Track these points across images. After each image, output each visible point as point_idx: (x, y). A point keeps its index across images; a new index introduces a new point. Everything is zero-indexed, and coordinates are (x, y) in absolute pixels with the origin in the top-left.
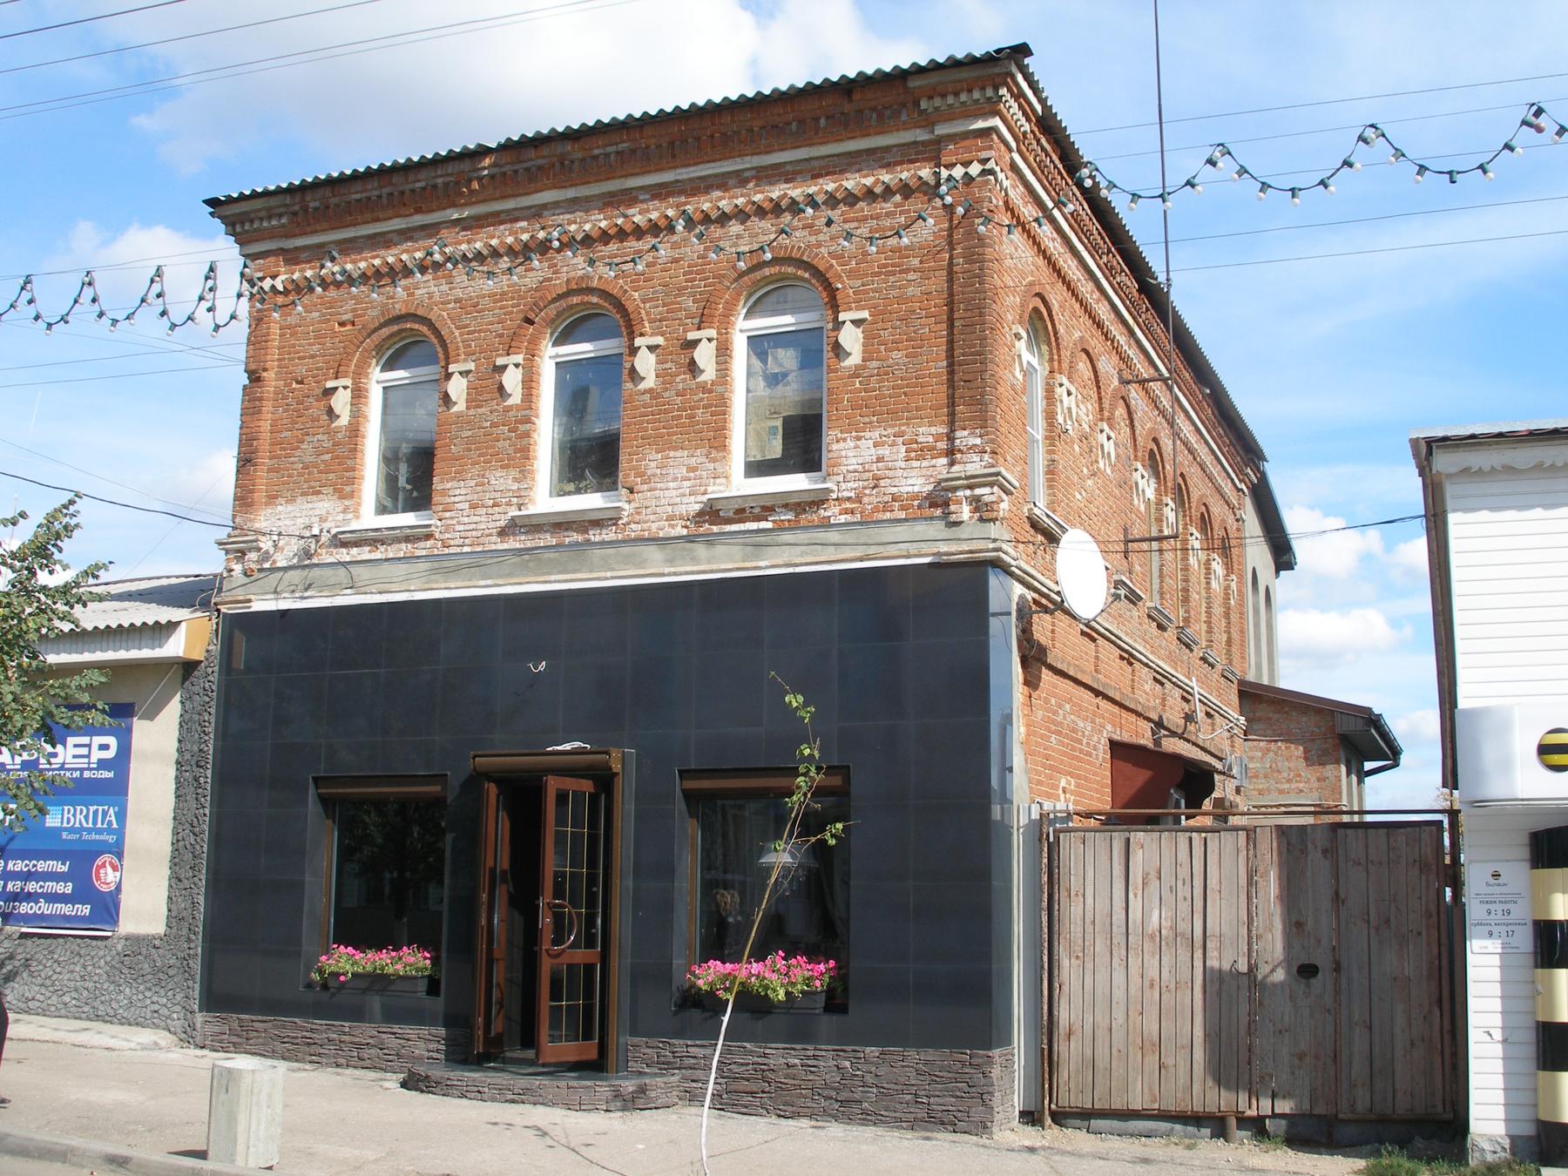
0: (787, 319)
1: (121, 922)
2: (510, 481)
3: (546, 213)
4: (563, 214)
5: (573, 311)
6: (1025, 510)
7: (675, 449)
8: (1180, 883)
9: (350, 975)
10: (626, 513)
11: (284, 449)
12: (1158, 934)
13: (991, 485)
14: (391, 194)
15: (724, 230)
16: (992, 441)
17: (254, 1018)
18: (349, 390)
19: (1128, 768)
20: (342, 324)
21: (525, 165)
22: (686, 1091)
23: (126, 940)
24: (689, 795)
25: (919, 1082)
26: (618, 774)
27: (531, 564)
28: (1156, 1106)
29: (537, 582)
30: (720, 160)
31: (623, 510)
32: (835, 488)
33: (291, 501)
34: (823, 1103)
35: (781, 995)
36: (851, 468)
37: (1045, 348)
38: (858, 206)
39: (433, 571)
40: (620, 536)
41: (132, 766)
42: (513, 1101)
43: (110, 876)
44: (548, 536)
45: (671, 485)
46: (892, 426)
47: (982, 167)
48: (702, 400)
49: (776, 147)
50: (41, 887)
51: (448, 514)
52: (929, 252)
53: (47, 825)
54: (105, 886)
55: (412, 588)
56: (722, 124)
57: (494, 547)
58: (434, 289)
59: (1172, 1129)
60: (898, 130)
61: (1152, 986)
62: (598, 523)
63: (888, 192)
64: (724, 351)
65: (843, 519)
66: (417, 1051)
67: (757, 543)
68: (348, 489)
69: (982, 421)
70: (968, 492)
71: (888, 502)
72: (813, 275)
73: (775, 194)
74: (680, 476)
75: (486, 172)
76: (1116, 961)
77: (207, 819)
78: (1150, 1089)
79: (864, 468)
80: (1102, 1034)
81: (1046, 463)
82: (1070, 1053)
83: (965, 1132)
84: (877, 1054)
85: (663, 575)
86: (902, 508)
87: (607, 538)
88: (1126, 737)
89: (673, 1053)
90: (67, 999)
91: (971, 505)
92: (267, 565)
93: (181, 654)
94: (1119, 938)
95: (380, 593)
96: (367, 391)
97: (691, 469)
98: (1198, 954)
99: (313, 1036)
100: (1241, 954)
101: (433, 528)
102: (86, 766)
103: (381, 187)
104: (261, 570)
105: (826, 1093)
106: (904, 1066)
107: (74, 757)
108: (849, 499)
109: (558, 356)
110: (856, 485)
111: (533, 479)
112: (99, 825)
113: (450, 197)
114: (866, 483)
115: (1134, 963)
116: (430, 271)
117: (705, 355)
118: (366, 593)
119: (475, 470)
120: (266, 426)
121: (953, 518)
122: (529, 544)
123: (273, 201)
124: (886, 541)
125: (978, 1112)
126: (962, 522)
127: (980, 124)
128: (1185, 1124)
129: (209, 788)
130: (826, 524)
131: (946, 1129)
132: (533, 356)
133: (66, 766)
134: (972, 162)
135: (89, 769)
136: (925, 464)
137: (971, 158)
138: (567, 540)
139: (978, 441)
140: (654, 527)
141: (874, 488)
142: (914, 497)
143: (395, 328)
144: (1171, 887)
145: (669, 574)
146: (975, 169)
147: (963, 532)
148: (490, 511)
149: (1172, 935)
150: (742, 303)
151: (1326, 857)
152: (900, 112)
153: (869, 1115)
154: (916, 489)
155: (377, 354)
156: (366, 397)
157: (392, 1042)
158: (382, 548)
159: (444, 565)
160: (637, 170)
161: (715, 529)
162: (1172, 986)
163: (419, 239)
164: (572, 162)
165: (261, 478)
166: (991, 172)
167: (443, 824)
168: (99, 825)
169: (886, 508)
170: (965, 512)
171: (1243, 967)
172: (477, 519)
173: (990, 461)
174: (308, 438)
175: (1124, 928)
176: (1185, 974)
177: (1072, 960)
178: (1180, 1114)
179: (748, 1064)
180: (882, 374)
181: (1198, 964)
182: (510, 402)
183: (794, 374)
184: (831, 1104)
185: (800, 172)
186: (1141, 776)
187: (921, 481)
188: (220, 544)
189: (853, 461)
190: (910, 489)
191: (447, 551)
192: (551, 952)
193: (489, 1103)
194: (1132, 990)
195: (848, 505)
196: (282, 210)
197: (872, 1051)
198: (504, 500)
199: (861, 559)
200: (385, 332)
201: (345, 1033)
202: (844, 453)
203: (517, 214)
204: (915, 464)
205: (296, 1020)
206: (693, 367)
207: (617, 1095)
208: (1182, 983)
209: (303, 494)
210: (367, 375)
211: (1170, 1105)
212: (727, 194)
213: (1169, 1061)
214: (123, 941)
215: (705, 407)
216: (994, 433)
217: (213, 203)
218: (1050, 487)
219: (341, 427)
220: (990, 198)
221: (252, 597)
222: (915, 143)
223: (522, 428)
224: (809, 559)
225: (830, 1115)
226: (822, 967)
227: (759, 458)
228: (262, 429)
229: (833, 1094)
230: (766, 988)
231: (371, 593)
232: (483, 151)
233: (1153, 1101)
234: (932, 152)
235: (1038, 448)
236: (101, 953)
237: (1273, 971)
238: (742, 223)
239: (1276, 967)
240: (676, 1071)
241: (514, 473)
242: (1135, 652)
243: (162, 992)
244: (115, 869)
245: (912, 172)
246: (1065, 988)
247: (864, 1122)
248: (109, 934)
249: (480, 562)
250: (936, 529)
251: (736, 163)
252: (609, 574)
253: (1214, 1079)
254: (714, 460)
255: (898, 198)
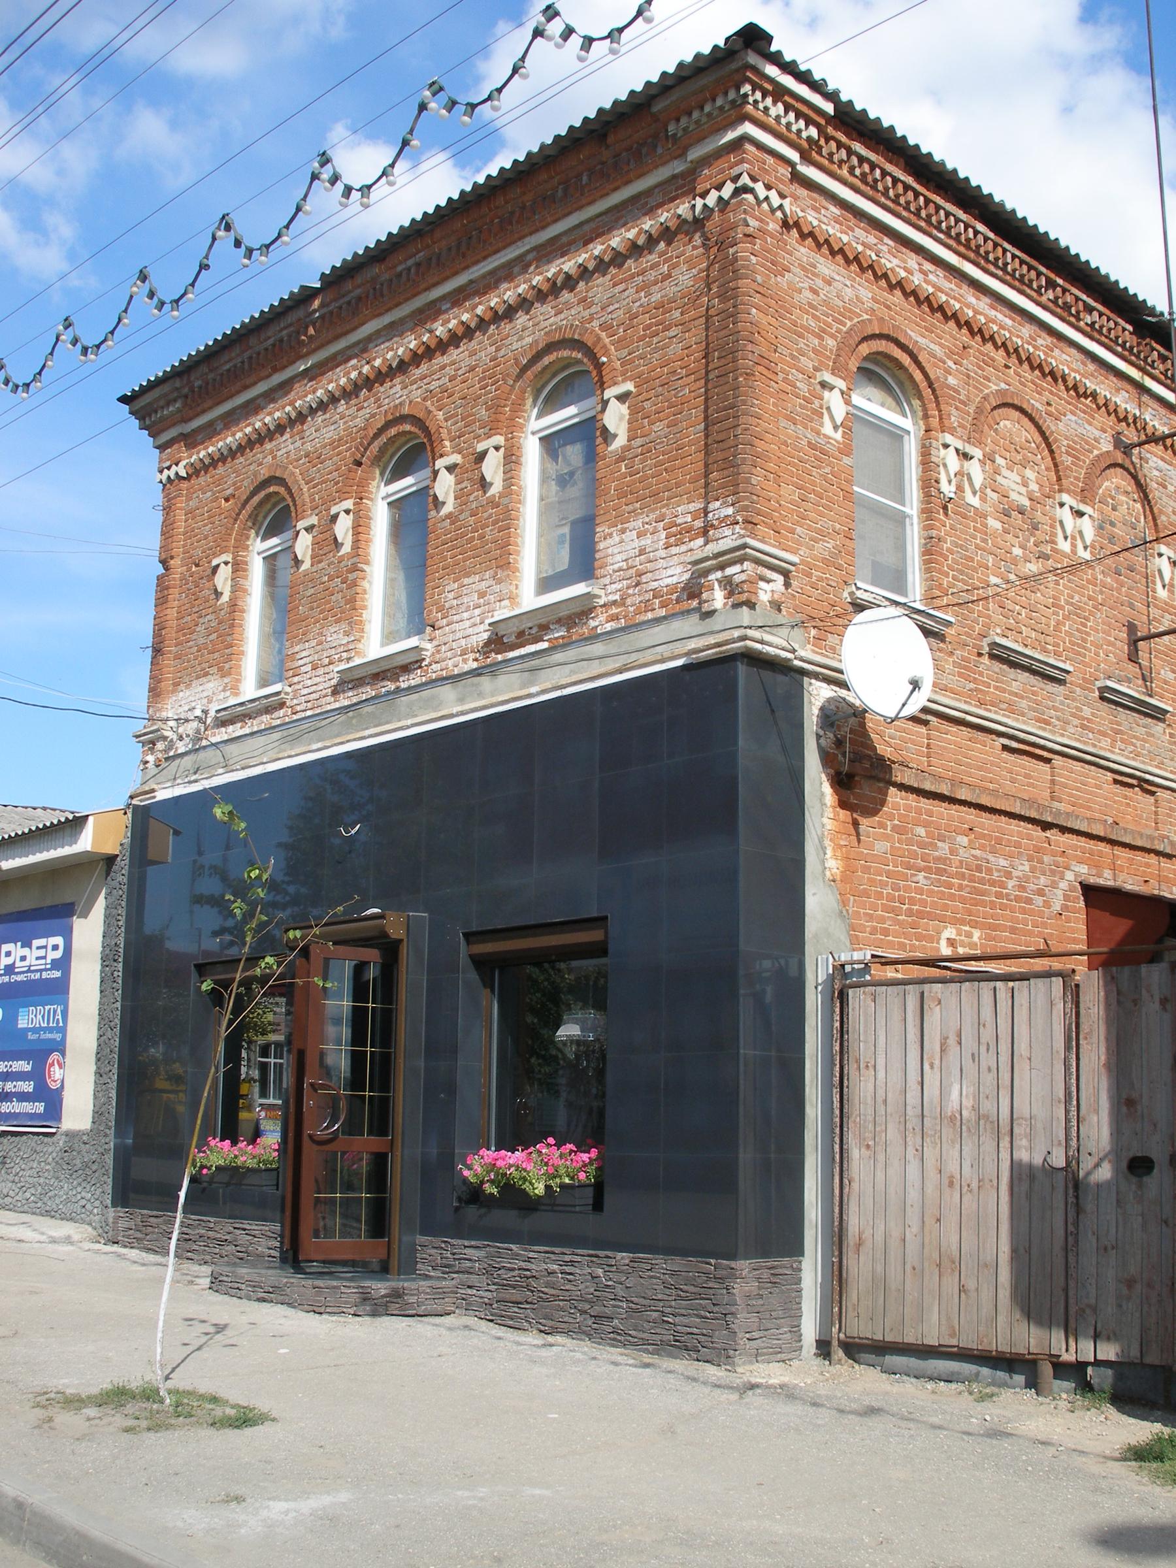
0: (572, 410)
1: (63, 1120)
2: (341, 636)
3: (371, 345)
4: (383, 343)
5: (397, 444)
6: (846, 594)
7: (468, 575)
8: (983, 1049)
9: (214, 1168)
10: (428, 654)
11: (184, 635)
12: (959, 1117)
13: (741, 560)
14: (250, 358)
15: (512, 325)
16: (745, 509)
17: (466, 1243)
18: (230, 565)
19: (1106, 918)
20: (227, 500)
21: (346, 299)
22: (463, 1299)
23: (67, 1135)
24: (479, 962)
25: (666, 1297)
26: (402, 940)
27: (354, 721)
28: (954, 1342)
29: (355, 740)
30: (504, 248)
31: (423, 649)
32: (602, 593)
33: (188, 686)
34: (579, 1318)
35: (540, 1189)
36: (616, 567)
37: (916, 403)
38: (626, 265)
39: (284, 740)
40: (424, 679)
41: (73, 964)
42: (263, 1300)
43: (57, 1072)
44: (368, 689)
45: (466, 615)
46: (653, 510)
47: (734, 186)
48: (490, 516)
49: (549, 220)
50: (15, 1086)
51: (296, 679)
52: (692, 299)
53: (19, 1026)
54: (54, 1084)
55: (265, 760)
56: (497, 208)
57: (329, 707)
58: (291, 447)
59: (977, 1374)
60: (656, 167)
61: (951, 1184)
62: (406, 669)
63: (652, 241)
64: (512, 459)
65: (609, 627)
66: (260, 1249)
67: (533, 667)
68: (227, 666)
69: (734, 487)
70: (719, 574)
71: (649, 600)
72: (585, 355)
73: (551, 271)
74: (472, 603)
75: (317, 315)
76: (911, 1151)
77: (119, 1013)
78: (949, 1319)
79: (627, 564)
80: (894, 1244)
81: (923, 541)
82: (859, 1268)
83: (707, 1362)
84: (627, 1261)
85: (452, 716)
86: (663, 605)
87: (413, 683)
88: (1106, 879)
89: (454, 1254)
90: (28, 1195)
91: (725, 589)
92: (171, 754)
93: (89, 849)
94: (913, 1122)
95: (243, 769)
96: (246, 563)
97: (482, 595)
98: (1005, 1143)
99: (529, 1266)
100: (1055, 1142)
101: (283, 695)
102: (43, 967)
103: (244, 352)
104: (167, 759)
105: (581, 1306)
106: (652, 1277)
107: (38, 958)
108: (614, 603)
109: (388, 496)
110: (621, 585)
111: (362, 631)
112: (51, 1025)
113: (287, 351)
114: (629, 582)
115: (930, 1154)
116: (288, 430)
117: (492, 467)
118: (233, 771)
119: (316, 629)
120: (172, 613)
121: (706, 607)
122: (355, 700)
123: (166, 388)
124: (646, 645)
125: (720, 1336)
126: (714, 611)
127: (730, 136)
128: (995, 1367)
129: (120, 982)
130: (594, 637)
131: (689, 1355)
132: (361, 499)
133: (32, 968)
134: (724, 183)
135: (46, 970)
136: (684, 548)
137: (724, 179)
138: (383, 690)
139: (730, 511)
140: (450, 663)
141: (637, 585)
142: (672, 589)
143: (262, 494)
144: (973, 1055)
145: (457, 715)
146: (727, 191)
147: (716, 623)
148: (327, 670)
149: (974, 1118)
150: (529, 402)
151: (1165, 1009)
152: (656, 146)
153: (619, 1334)
154: (674, 580)
155: (254, 524)
156: (245, 570)
157: (244, 1238)
158: (249, 722)
159: (293, 732)
160: (436, 279)
161: (500, 657)
162: (975, 1185)
163: (279, 399)
164: (382, 285)
165: (168, 666)
166: (746, 189)
167: (569, 1031)
168: (51, 1025)
169: (647, 606)
170: (718, 598)
171: (1059, 1161)
172: (318, 680)
173: (742, 532)
174: (201, 620)
175: (920, 1108)
176: (990, 1169)
177: (863, 1150)
178: (984, 1354)
179: (513, 1270)
180: (646, 451)
181: (1005, 1156)
182: (342, 552)
183: (580, 472)
184: (585, 1319)
185: (570, 243)
186: (1121, 926)
187: (679, 570)
188: (137, 737)
189: (619, 558)
190: (669, 581)
191: (295, 717)
192: (315, 1138)
193: (244, 1301)
194: (929, 1189)
195: (614, 610)
196: (175, 394)
197: (623, 1257)
198: (336, 657)
199: (620, 671)
200: (256, 499)
201: (211, 1229)
202: (610, 551)
203: (349, 353)
204: (674, 550)
205: (512, 1246)
206: (484, 484)
207: (365, 1298)
208: (987, 1181)
209: (198, 678)
210: (246, 548)
211: (969, 1341)
212: (512, 284)
213: (971, 1284)
214: (64, 1137)
215: (495, 523)
216: (746, 498)
217: (124, 399)
218: (928, 570)
219: (223, 604)
220: (745, 220)
221: (156, 787)
222: (674, 177)
223: (351, 576)
224: (574, 678)
225: (584, 1333)
226: (585, 1157)
227: (550, 573)
228: (168, 617)
229: (587, 1306)
230: (525, 1179)
231: (237, 770)
232: (306, 295)
233: (952, 1335)
234: (685, 185)
235: (912, 524)
236: (50, 1150)
237: (1097, 1165)
238: (527, 313)
239: (1102, 1160)
240: (455, 1275)
241: (344, 626)
242: (1148, 777)
243: (88, 1187)
244: (60, 1066)
245: (672, 211)
246: (855, 1185)
247: (615, 1343)
248: (53, 1130)
249: (318, 723)
250: (688, 625)
251: (518, 247)
252: (409, 722)
253: (1022, 1310)
254: (499, 582)
255: (662, 245)
